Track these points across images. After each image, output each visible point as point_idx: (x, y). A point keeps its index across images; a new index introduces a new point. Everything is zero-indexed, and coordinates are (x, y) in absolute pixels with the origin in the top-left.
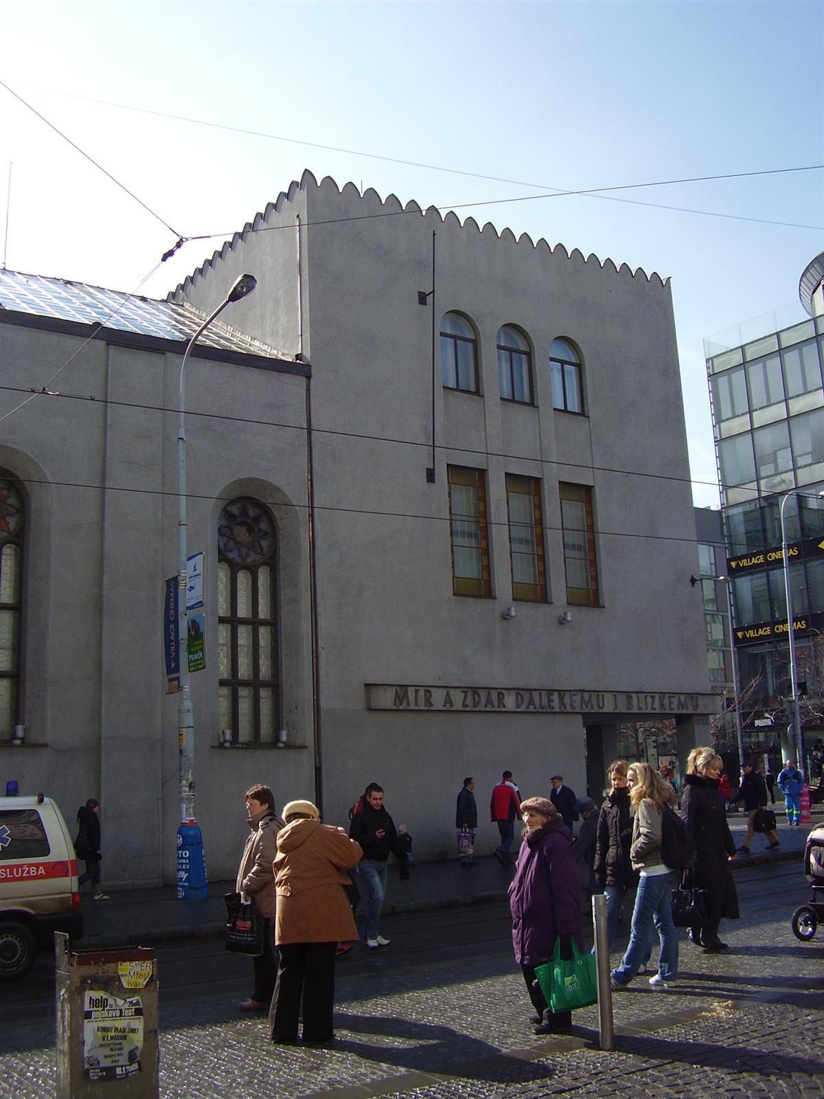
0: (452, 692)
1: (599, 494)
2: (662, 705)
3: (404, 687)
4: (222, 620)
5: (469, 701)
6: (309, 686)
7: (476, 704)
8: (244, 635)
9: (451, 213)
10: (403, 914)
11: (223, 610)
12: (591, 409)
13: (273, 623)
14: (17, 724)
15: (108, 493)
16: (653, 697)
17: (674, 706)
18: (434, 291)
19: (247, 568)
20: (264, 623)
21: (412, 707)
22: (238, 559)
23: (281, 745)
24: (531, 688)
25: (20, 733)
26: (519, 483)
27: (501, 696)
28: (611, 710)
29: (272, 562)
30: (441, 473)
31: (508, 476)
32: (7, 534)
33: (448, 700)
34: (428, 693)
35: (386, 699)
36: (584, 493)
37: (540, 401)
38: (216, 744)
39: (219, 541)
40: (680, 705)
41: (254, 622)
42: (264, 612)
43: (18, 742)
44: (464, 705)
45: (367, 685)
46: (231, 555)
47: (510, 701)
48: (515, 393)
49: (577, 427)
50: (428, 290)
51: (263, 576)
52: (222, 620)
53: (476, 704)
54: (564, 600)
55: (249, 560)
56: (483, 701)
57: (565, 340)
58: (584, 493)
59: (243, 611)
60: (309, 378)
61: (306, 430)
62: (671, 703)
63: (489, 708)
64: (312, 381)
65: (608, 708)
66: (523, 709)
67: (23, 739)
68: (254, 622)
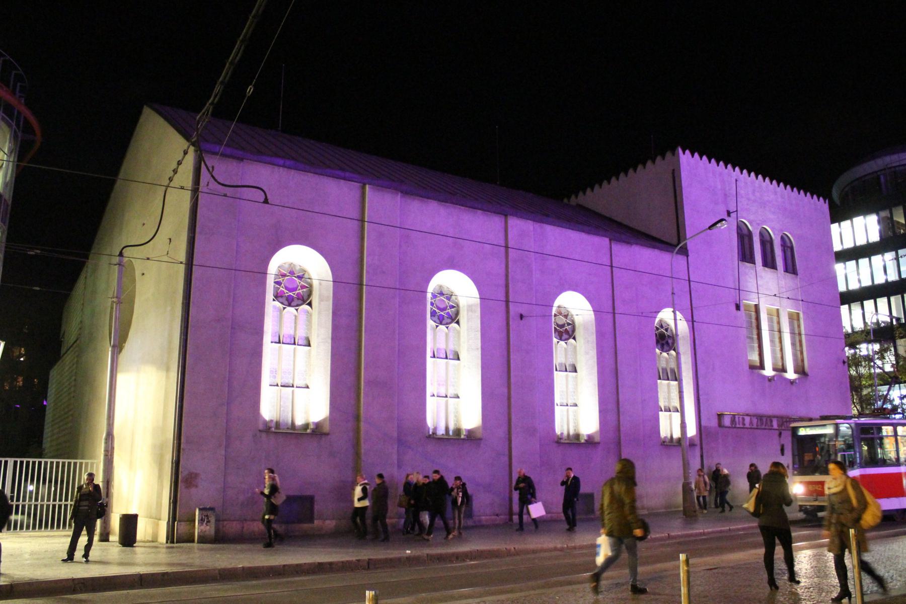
5: (759, 423)
18: (737, 211)
27: (771, 421)
33: (751, 423)
56: (764, 423)
60: (687, 256)
63: (767, 427)
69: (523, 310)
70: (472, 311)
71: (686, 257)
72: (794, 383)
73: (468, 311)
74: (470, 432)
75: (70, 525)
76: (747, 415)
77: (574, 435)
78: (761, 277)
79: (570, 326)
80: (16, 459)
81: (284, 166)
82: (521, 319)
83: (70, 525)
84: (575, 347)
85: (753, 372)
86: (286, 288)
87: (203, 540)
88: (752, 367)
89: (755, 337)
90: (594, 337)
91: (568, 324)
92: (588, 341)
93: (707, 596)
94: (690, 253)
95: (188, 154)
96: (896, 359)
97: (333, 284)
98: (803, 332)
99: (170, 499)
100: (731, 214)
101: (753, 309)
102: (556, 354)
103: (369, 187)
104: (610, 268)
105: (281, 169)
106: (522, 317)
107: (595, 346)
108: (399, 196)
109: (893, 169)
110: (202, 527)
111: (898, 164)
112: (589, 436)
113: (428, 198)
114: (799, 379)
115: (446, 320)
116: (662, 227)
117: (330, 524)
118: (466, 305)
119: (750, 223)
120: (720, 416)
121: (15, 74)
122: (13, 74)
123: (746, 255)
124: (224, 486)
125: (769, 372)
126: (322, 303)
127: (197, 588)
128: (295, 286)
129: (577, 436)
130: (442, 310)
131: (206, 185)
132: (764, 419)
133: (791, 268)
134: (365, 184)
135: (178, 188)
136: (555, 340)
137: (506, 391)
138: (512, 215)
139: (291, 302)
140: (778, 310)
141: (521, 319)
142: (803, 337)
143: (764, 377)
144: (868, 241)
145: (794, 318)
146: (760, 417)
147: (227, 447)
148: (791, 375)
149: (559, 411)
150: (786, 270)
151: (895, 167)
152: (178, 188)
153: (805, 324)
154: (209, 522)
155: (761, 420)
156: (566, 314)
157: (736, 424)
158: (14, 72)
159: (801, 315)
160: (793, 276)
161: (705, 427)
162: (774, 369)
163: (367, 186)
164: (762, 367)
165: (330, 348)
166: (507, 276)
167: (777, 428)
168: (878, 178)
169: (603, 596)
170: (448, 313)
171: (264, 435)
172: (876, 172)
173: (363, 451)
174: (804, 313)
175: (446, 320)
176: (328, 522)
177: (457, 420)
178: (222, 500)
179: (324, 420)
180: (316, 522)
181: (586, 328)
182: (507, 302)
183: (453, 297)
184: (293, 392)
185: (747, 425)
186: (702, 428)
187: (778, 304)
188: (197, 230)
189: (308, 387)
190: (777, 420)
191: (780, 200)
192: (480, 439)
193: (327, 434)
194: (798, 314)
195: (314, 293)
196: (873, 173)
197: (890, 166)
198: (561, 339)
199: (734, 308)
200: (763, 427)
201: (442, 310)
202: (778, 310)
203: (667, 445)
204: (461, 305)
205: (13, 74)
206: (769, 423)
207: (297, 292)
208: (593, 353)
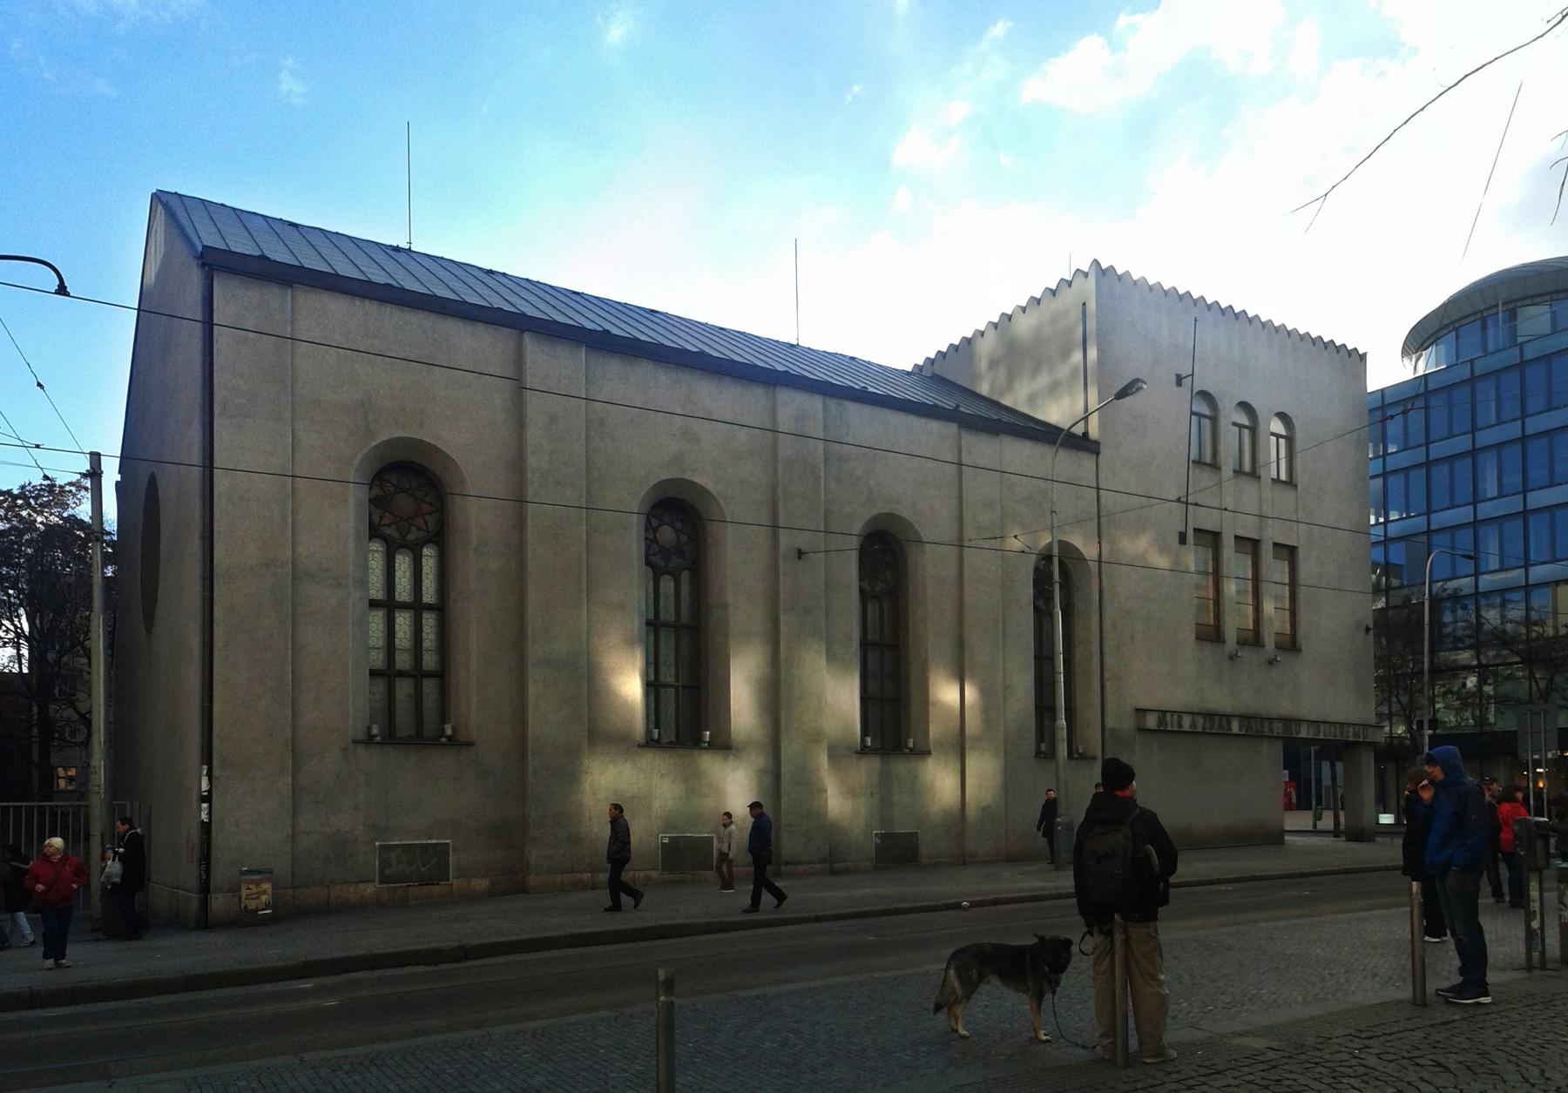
0: (1196, 717)
1: (1301, 553)
2: (1341, 734)
3: (1164, 712)
4: (374, 604)
5: (1207, 724)
6: (1098, 710)
7: (1212, 726)
8: (403, 621)
9: (1343, 347)
10: (81, 963)
11: (377, 592)
12: (1300, 478)
13: (441, 608)
14: (444, 723)
15: (966, 551)
16: (1335, 727)
17: (1351, 734)
18: (1192, 375)
19: (670, 573)
20: (429, 607)
21: (1169, 728)
22: (396, 535)
23: (1076, 756)
24: (1302, 718)
25: (449, 732)
26: (1250, 545)
27: (1229, 723)
28: (1305, 736)
29: (440, 537)
30: (1190, 534)
31: (1236, 537)
32: (426, 534)
33: (1193, 724)
34: (1180, 719)
35: (1151, 722)
36: (1289, 552)
37: (1262, 472)
38: (361, 736)
39: (370, 513)
40: (1356, 734)
41: (417, 607)
42: (429, 594)
43: (444, 740)
44: (1204, 729)
45: (1137, 710)
46: (388, 531)
47: (1235, 727)
48: (1390, 495)
49: (1288, 495)
50: (1185, 371)
51: (685, 576)
52: (374, 604)
53: (1212, 726)
54: (1273, 645)
55: (411, 537)
56: (1216, 725)
57: (1245, 406)
58: (1289, 552)
59: (403, 591)
60: (1098, 454)
61: (200, 325)
62: (1348, 732)
64: (1100, 456)
65: (1303, 734)
66: (1243, 733)
67: (450, 738)
68: (417, 607)
69: (803, 541)
71: (1095, 456)
72: (1274, 662)
82: (800, 558)
93: (1222, 994)
95: (1205, 389)
96: (368, 563)
104: (1101, 486)
108: (584, 350)
120: (1141, 712)
124: (293, 832)
135: (1074, 425)
139: (407, 534)
141: (800, 558)
146: (1209, 715)
147: (296, 768)
152: (1074, 425)
157: (1166, 726)
161: (1113, 730)
166: (960, 497)
169: (1159, 990)
171: (361, 749)
173: (530, 770)
178: (290, 855)
182: (775, 527)
186: (1107, 733)
188: (217, 410)
190: (1240, 721)
206: (1225, 725)
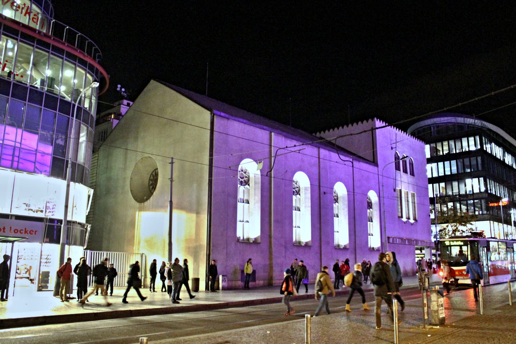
27: (406, 241)
60: (378, 167)
70: (307, 190)
73: (305, 190)
74: (307, 243)
75: (92, 285)
76: (399, 238)
77: (298, 241)
78: (402, 177)
79: (247, 178)
80: (107, 252)
81: (243, 123)
83: (92, 285)
84: (300, 199)
85: (399, 220)
86: (240, 177)
87: (224, 289)
88: (399, 217)
89: (399, 203)
90: (347, 202)
91: (297, 187)
92: (344, 204)
94: (379, 166)
97: (261, 177)
98: (416, 202)
99: (206, 271)
100: (393, 149)
101: (399, 191)
102: (335, 210)
103: (274, 134)
105: (242, 123)
106: (325, 193)
107: (347, 206)
109: (437, 125)
110: (223, 283)
111: (439, 122)
112: (306, 243)
113: (292, 139)
114: (414, 222)
115: (244, 184)
116: (368, 154)
117: (261, 282)
118: (304, 187)
119: (399, 153)
120: (389, 238)
121: (98, 55)
122: (97, 55)
123: (398, 168)
125: (404, 219)
126: (256, 185)
127: (106, 322)
128: (243, 177)
129: (300, 242)
130: (242, 178)
131: (11, 64)
132: (403, 240)
133: (412, 174)
134: (271, 132)
136: (239, 185)
137: (319, 225)
138: (322, 148)
140: (407, 192)
142: (416, 205)
143: (403, 221)
144: (472, 180)
145: (413, 195)
148: (412, 221)
149: (239, 225)
150: (410, 174)
151: (438, 123)
153: (417, 199)
154: (225, 281)
155: (402, 240)
156: (245, 171)
158: (97, 54)
159: (415, 195)
160: (413, 177)
162: (407, 218)
163: (273, 134)
164: (402, 217)
165: (260, 205)
167: (408, 244)
168: (430, 128)
170: (296, 190)
172: (430, 125)
174: (417, 193)
175: (244, 184)
176: (260, 281)
177: (299, 238)
179: (259, 237)
180: (257, 282)
181: (343, 198)
183: (298, 183)
184: (243, 224)
185: (398, 243)
187: (408, 189)
189: (248, 222)
191: (409, 142)
192: (311, 246)
193: (259, 243)
194: (414, 194)
195: (250, 180)
196: (428, 125)
197: (436, 123)
198: (241, 185)
199: (393, 191)
200: (403, 243)
201: (242, 178)
202: (407, 192)
203: (336, 249)
204: (301, 187)
205: (97, 55)
207: (244, 179)
208: (346, 210)
